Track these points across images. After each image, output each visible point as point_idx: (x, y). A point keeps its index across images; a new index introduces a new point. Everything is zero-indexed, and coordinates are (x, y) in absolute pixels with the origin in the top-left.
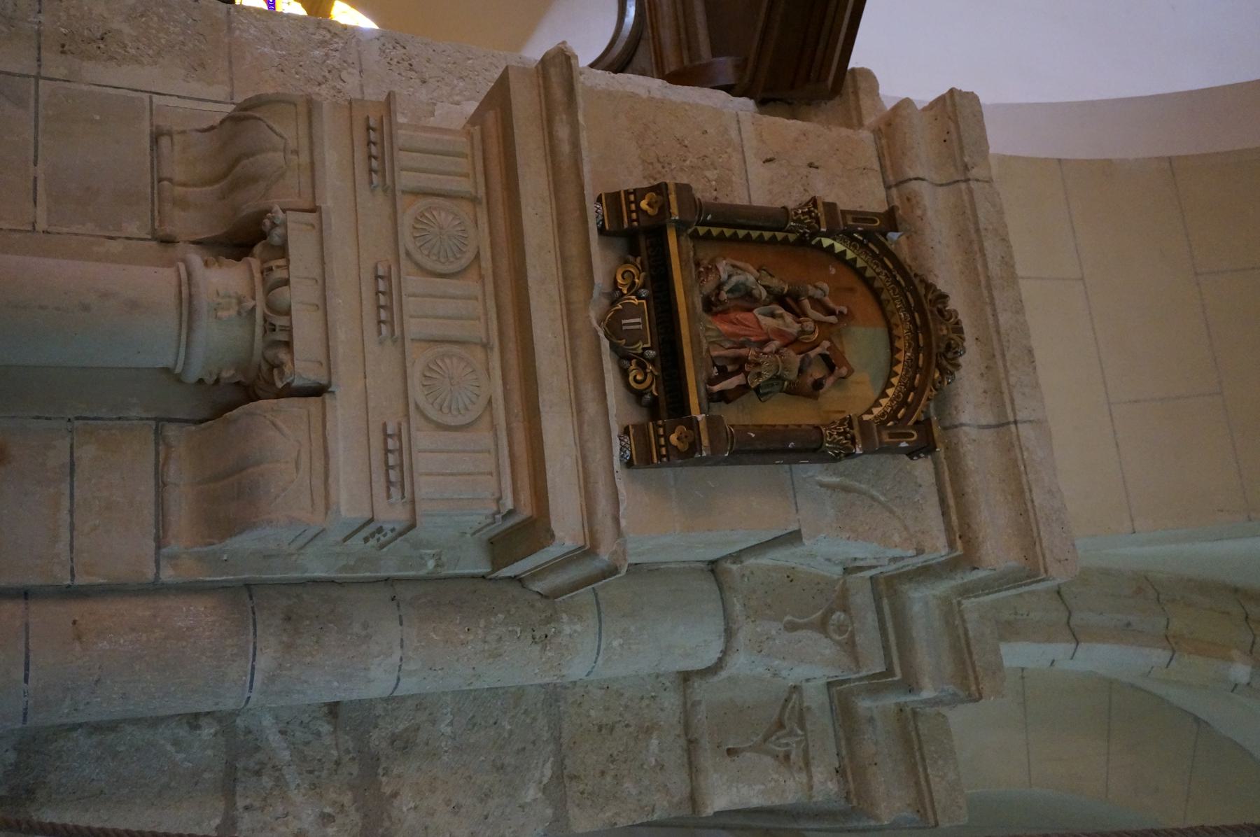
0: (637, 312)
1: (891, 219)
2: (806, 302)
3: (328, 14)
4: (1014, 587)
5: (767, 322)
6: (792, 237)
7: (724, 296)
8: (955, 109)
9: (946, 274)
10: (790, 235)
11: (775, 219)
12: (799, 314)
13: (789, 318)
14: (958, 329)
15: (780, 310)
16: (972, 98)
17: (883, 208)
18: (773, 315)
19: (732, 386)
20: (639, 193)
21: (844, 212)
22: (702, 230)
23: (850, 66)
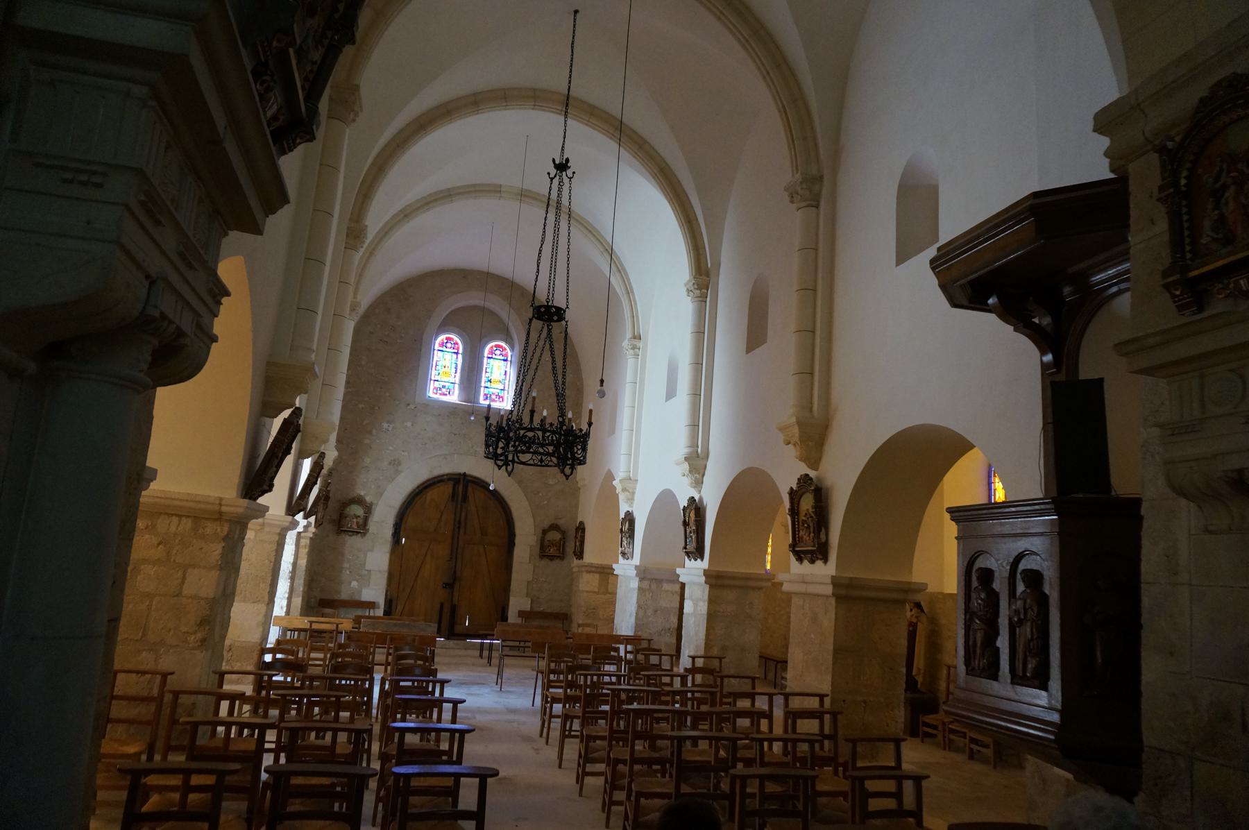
0: (1237, 283)
1: (1161, 150)
2: (1218, 186)
3: (1107, 486)
4: (295, 564)
5: (1231, 206)
6: (1184, 203)
7: (1221, 236)
8: (1105, 122)
9: (1188, 100)
10: (1181, 202)
11: (1174, 218)
12: (1225, 187)
13: (1227, 195)
14: (1218, 84)
15: (1223, 201)
16: (1097, 117)
17: (1156, 155)
18: (1227, 203)
19: (999, 644)
20: (1173, 296)
21: (1163, 179)
22: (1189, 255)
23: (1112, 176)
